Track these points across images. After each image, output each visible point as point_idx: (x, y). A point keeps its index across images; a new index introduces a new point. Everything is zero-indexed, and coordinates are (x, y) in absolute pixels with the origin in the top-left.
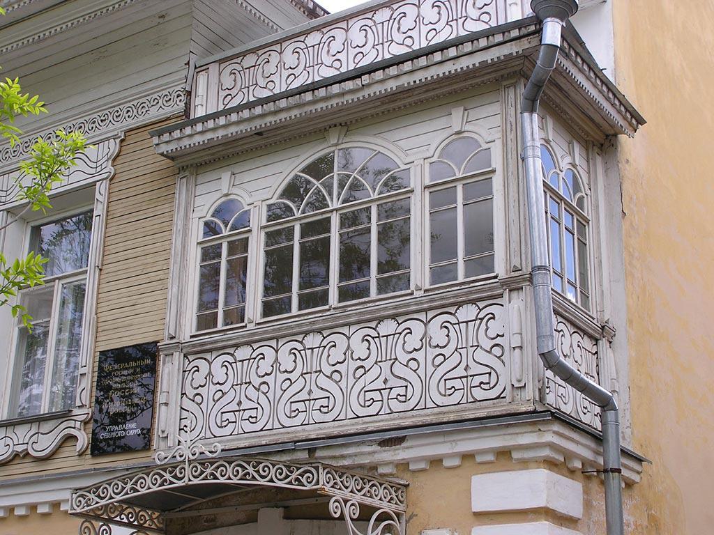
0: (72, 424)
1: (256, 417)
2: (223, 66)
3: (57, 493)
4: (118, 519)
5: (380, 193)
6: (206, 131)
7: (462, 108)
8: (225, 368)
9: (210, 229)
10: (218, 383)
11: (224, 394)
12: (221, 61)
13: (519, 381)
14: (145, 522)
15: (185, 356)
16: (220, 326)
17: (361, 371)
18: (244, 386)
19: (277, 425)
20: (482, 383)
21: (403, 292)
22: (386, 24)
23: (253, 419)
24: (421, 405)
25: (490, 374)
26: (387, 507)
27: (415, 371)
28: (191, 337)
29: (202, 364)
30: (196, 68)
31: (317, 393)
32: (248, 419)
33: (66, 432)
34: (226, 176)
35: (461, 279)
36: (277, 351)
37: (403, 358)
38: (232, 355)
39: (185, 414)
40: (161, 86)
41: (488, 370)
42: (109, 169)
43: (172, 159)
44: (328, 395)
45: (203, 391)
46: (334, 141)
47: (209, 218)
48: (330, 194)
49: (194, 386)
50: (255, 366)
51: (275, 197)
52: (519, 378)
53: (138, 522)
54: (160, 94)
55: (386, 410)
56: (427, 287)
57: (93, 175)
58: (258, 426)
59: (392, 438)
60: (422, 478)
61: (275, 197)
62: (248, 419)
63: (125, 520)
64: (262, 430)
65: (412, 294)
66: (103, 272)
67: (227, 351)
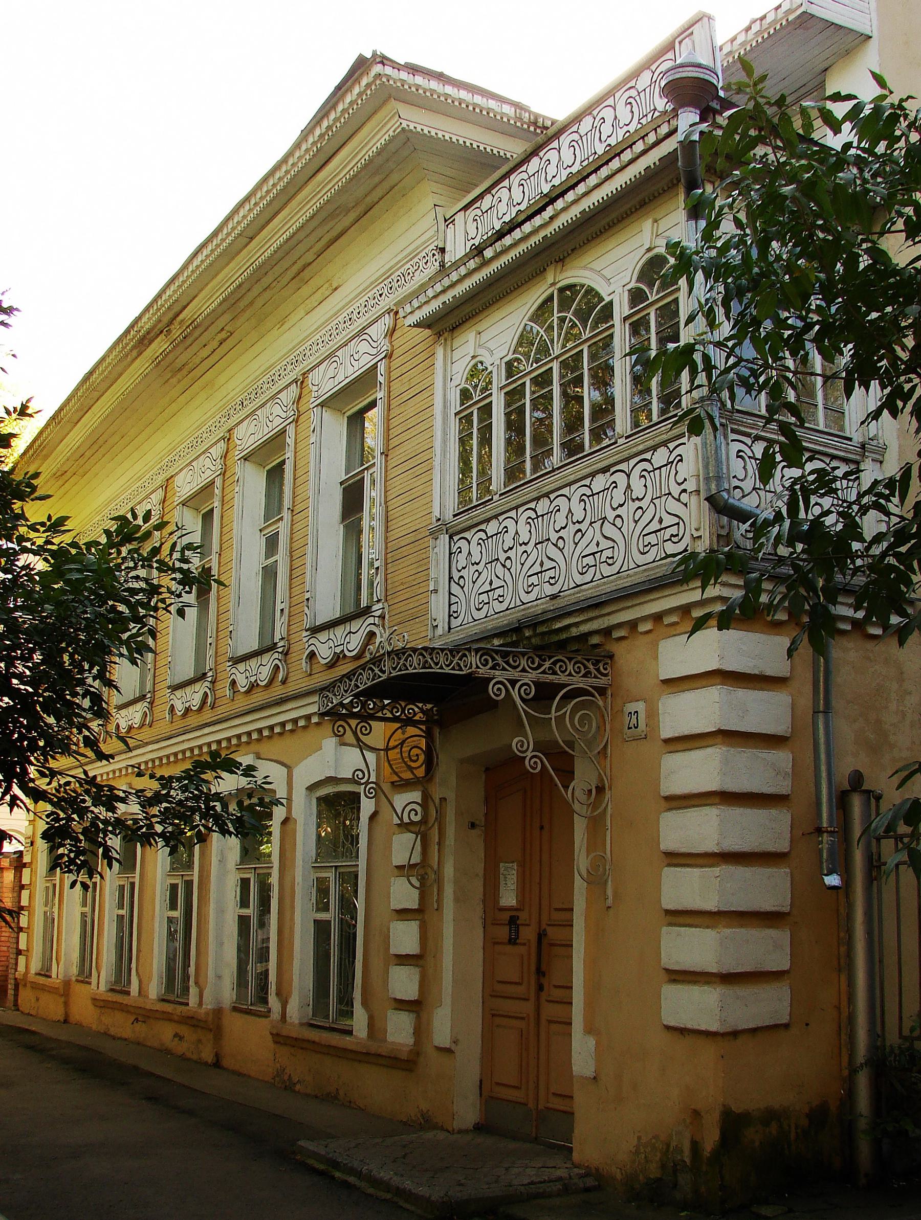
0: (371, 620)
1: (613, 558)
2: (468, 212)
3: (237, 728)
4: (380, 714)
5: (564, 346)
6: (579, 199)
7: (650, 221)
8: (582, 503)
9: (465, 395)
10: (637, 499)
11: (480, 574)
12: (465, 208)
13: (697, 530)
14: (415, 714)
15: (451, 537)
16: (587, 450)
17: (640, 512)
18: (494, 564)
19: (471, 620)
20: (672, 535)
21: (581, 455)
22: (648, 90)
23: (500, 599)
24: (625, 568)
25: (678, 524)
26: (579, 682)
27: (620, 529)
28: (455, 516)
29: (620, 478)
30: (446, 221)
31: (668, 520)
32: (670, 540)
33: (368, 629)
34: (647, 225)
35: (529, 477)
36: (628, 476)
37: (610, 515)
38: (649, 461)
39: (454, 599)
40: (425, 242)
41: (676, 520)
42: (386, 346)
43: (429, 327)
44: (554, 564)
45: (511, 554)
46: (550, 280)
47: (633, 285)
48: (552, 341)
49: (615, 506)
50: (673, 472)
51: (511, 353)
52: (697, 527)
53: (405, 715)
54: (419, 257)
55: (598, 576)
56: (629, 433)
57: (376, 355)
58: (504, 606)
59: (597, 605)
60: (624, 644)
61: (511, 353)
62: (670, 540)
63: (389, 715)
64: (507, 609)
65: (616, 443)
66: (389, 458)
67: (583, 483)
